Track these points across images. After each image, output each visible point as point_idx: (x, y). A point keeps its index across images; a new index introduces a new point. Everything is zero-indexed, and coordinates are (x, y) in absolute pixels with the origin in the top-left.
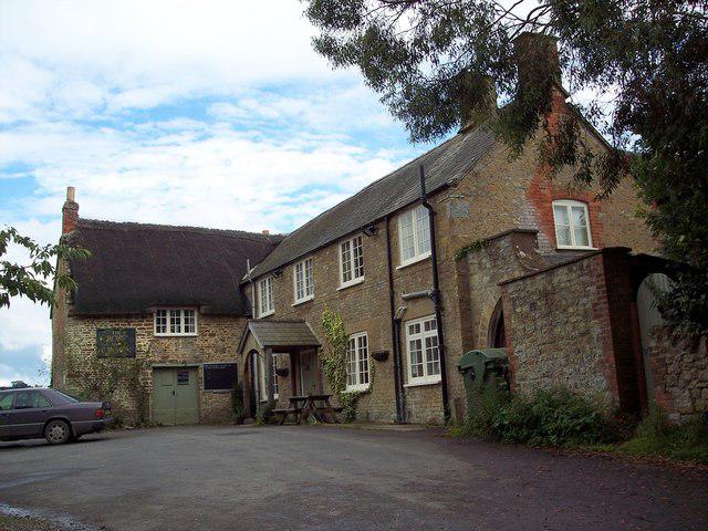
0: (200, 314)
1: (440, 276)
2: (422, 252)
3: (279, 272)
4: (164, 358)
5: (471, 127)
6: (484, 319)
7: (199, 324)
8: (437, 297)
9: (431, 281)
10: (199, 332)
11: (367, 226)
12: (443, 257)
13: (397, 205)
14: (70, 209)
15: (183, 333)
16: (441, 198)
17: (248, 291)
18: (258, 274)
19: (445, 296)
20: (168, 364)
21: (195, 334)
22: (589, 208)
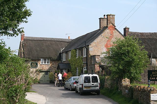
8: (87, 64)
15: (47, 64)
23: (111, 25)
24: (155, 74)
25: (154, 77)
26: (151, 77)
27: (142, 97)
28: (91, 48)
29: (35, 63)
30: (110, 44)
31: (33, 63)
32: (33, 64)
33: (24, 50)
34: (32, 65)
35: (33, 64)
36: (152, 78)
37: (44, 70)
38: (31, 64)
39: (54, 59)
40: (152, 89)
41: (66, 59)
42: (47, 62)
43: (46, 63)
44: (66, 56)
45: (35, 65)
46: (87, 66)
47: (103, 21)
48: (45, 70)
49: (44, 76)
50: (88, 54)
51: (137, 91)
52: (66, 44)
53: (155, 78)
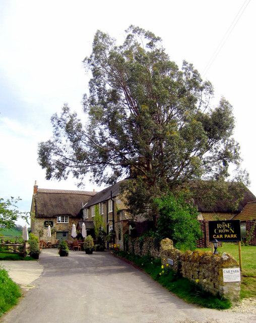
8: (113, 221)
15: (65, 222)
24: (222, 229)
25: (221, 234)
26: (215, 234)
27: (201, 273)
32: (46, 223)
34: (219, 229)
35: (46, 223)
36: (218, 236)
40: (225, 258)
41: (90, 215)
42: (65, 220)
44: (89, 213)
45: (227, 228)
46: (114, 224)
50: (115, 206)
51: (190, 261)
52: (87, 198)
53: (224, 236)
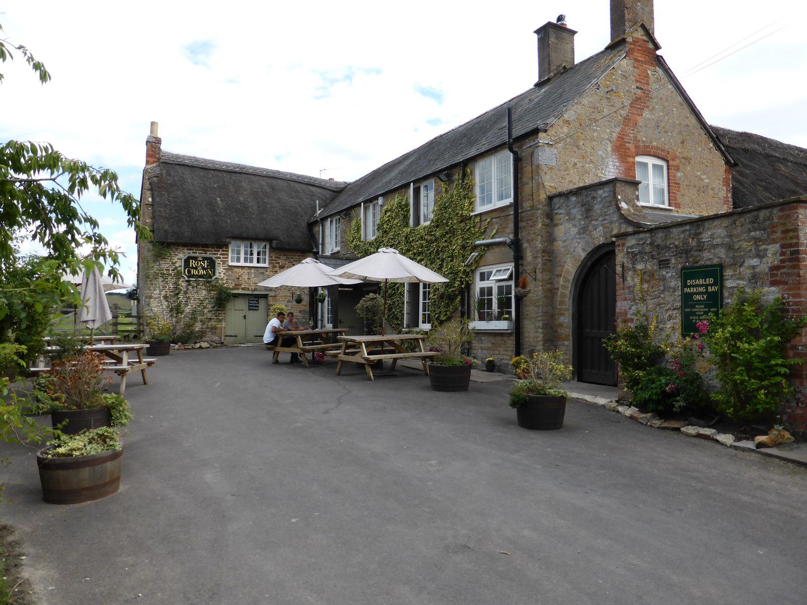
0: (271, 248)
1: (520, 224)
2: (501, 198)
3: (348, 213)
4: (237, 286)
5: (549, 80)
6: (568, 272)
7: (270, 257)
8: (516, 247)
9: (511, 226)
10: (270, 263)
11: (442, 170)
12: (527, 205)
13: (473, 152)
14: (153, 145)
15: (255, 264)
16: (528, 144)
17: (316, 229)
18: (326, 214)
19: (525, 245)
20: (240, 291)
21: (266, 265)
22: (668, 166)
23: (639, 34)
28: (547, 149)
29: (204, 259)
30: (635, 139)
31: (195, 258)
32: (192, 263)
33: (158, 199)
34: (193, 268)
35: (192, 263)
37: (243, 289)
38: (187, 262)
39: (287, 247)
43: (251, 261)
45: (203, 268)
47: (557, 38)
48: (248, 289)
49: (245, 317)
